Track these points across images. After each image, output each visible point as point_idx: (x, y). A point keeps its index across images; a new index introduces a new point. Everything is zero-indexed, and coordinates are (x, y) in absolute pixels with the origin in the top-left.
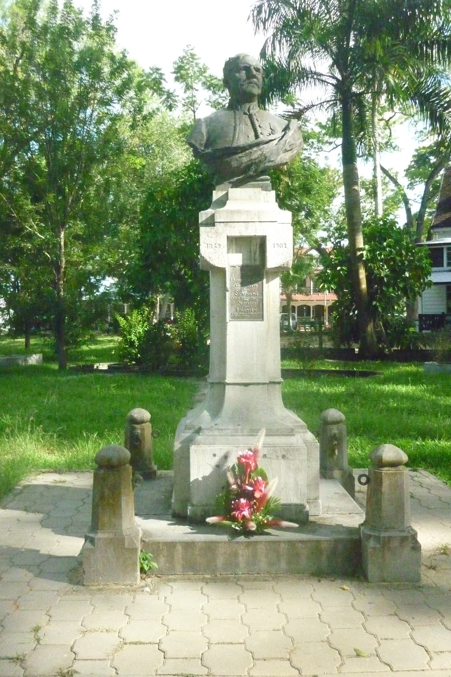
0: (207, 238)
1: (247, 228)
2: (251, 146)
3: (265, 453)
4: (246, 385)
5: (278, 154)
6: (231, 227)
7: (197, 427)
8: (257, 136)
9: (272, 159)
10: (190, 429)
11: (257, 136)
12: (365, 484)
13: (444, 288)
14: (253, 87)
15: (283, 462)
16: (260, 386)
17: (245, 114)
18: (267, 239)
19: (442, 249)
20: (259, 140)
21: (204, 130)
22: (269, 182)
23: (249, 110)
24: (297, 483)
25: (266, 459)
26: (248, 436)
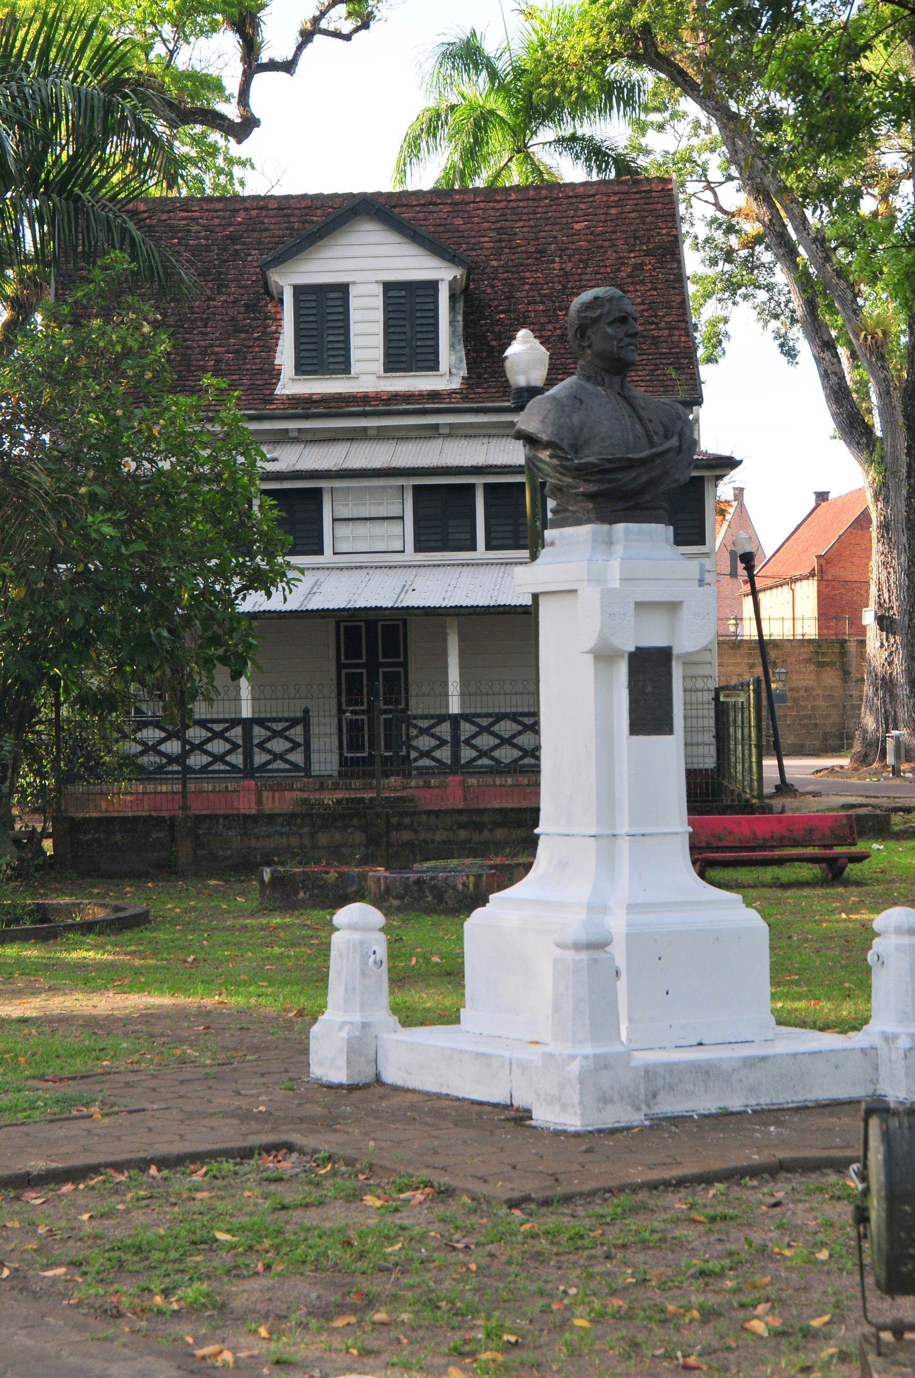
8: (652, 445)
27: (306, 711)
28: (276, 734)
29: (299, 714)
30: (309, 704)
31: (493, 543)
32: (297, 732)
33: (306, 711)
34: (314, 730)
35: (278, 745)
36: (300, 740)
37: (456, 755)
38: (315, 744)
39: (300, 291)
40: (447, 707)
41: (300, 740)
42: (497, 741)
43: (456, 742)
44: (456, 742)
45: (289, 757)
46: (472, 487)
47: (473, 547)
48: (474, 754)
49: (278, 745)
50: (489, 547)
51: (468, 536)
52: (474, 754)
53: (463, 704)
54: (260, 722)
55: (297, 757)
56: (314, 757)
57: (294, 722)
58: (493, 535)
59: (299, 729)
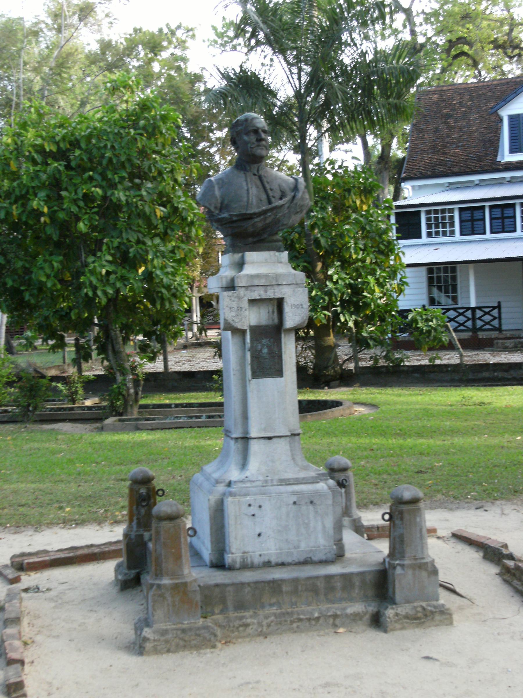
0: (230, 302)
1: (266, 291)
2: (265, 212)
3: (295, 500)
4: (270, 438)
5: (289, 217)
6: (251, 291)
7: (227, 481)
8: (270, 202)
9: (285, 223)
10: (221, 483)
11: (270, 202)
12: (159, 490)
13: (423, 270)
14: (262, 149)
15: (311, 507)
16: (282, 439)
17: (255, 175)
18: (285, 300)
19: (419, 212)
20: (273, 205)
21: (217, 193)
22: (281, 243)
23: (258, 171)
24: (324, 527)
25: (296, 506)
26: (277, 485)
27: (499, 303)
28: (486, 313)
29: (496, 304)
30: (500, 299)
31: (494, 231)
32: (495, 313)
33: (499, 303)
34: (503, 310)
35: (487, 318)
36: (496, 315)
37: (474, 324)
38: (503, 316)
39: (512, 118)
40: (469, 303)
41: (496, 315)
42: (456, 319)
43: (474, 319)
44: (474, 319)
45: (492, 323)
46: (419, 212)
47: (484, 233)
48: (482, 323)
49: (487, 318)
50: (462, 234)
51: (513, 226)
52: (482, 323)
53: (477, 303)
54: (480, 308)
55: (496, 323)
56: (503, 321)
57: (494, 308)
58: (513, 223)
59: (496, 311)
